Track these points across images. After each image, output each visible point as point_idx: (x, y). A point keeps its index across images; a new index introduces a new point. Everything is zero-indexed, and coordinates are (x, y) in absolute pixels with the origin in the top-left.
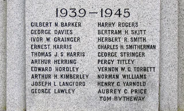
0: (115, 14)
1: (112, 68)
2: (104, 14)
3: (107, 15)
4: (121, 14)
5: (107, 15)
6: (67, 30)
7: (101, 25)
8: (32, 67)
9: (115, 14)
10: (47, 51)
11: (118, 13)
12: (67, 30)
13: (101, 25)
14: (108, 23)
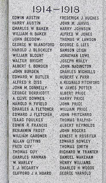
0: (47, 10)
1: (17, 72)
2: (64, 10)
3: (38, 11)
4: (51, 11)
5: (38, 11)
6: (41, 103)
7: (64, 168)
8: (13, 76)
9: (47, 10)
10: (71, 139)
11: (49, 10)
12: (41, 103)
13: (64, 168)
14: (22, 81)
